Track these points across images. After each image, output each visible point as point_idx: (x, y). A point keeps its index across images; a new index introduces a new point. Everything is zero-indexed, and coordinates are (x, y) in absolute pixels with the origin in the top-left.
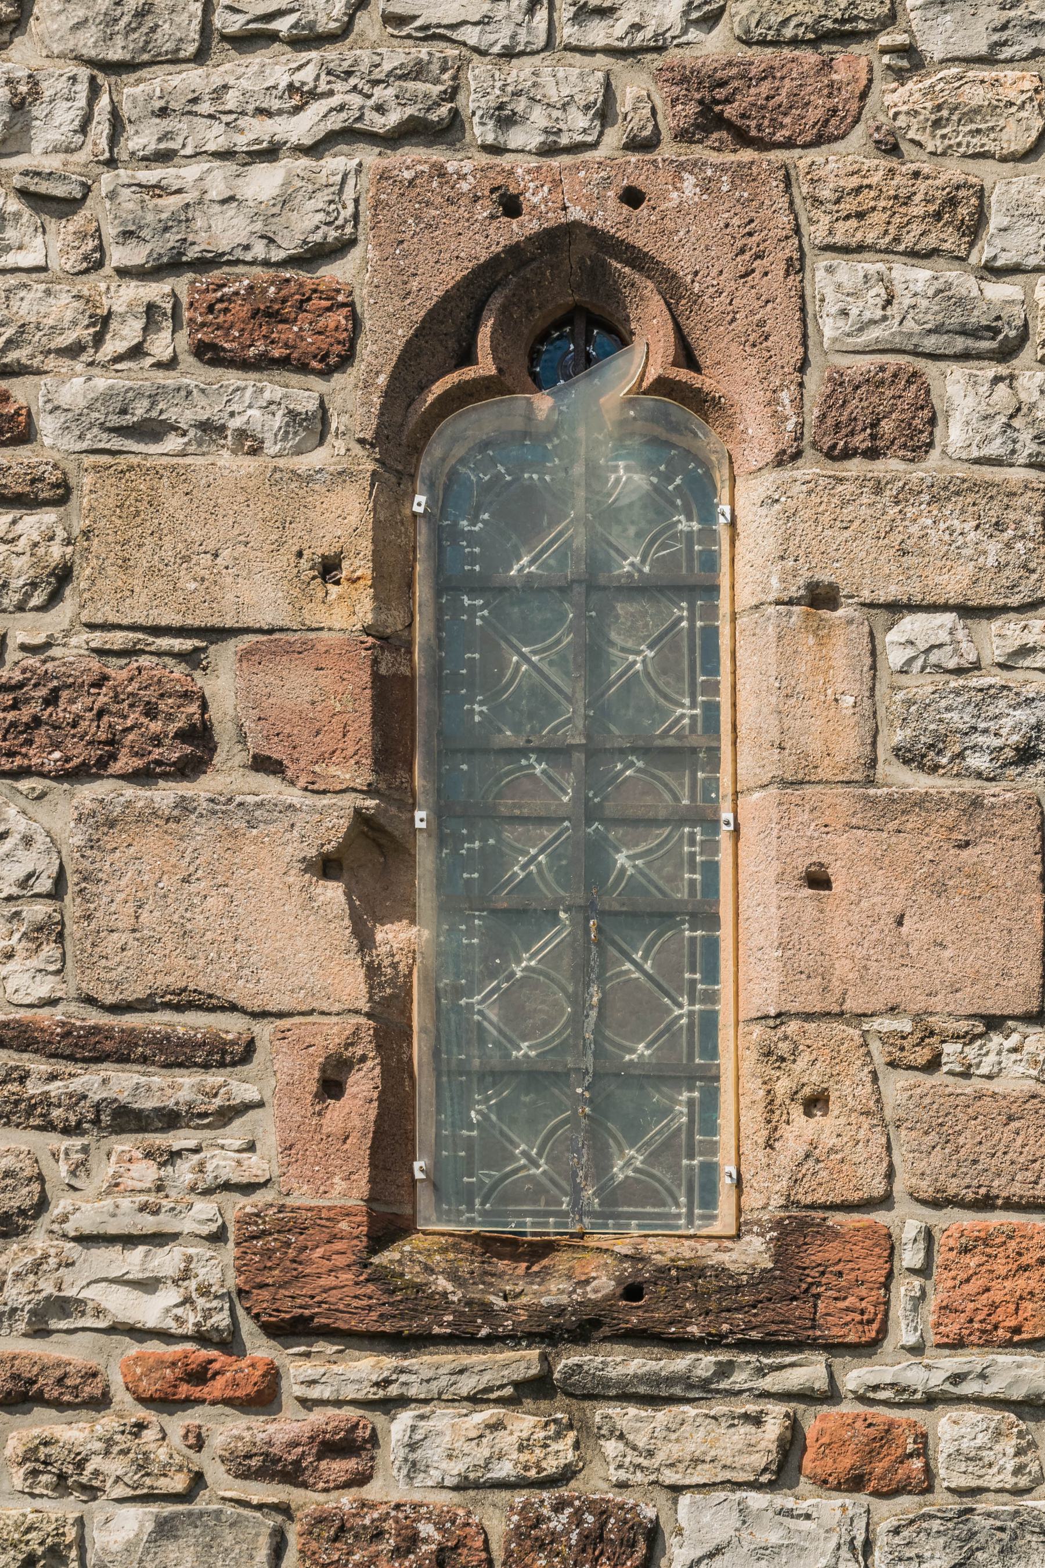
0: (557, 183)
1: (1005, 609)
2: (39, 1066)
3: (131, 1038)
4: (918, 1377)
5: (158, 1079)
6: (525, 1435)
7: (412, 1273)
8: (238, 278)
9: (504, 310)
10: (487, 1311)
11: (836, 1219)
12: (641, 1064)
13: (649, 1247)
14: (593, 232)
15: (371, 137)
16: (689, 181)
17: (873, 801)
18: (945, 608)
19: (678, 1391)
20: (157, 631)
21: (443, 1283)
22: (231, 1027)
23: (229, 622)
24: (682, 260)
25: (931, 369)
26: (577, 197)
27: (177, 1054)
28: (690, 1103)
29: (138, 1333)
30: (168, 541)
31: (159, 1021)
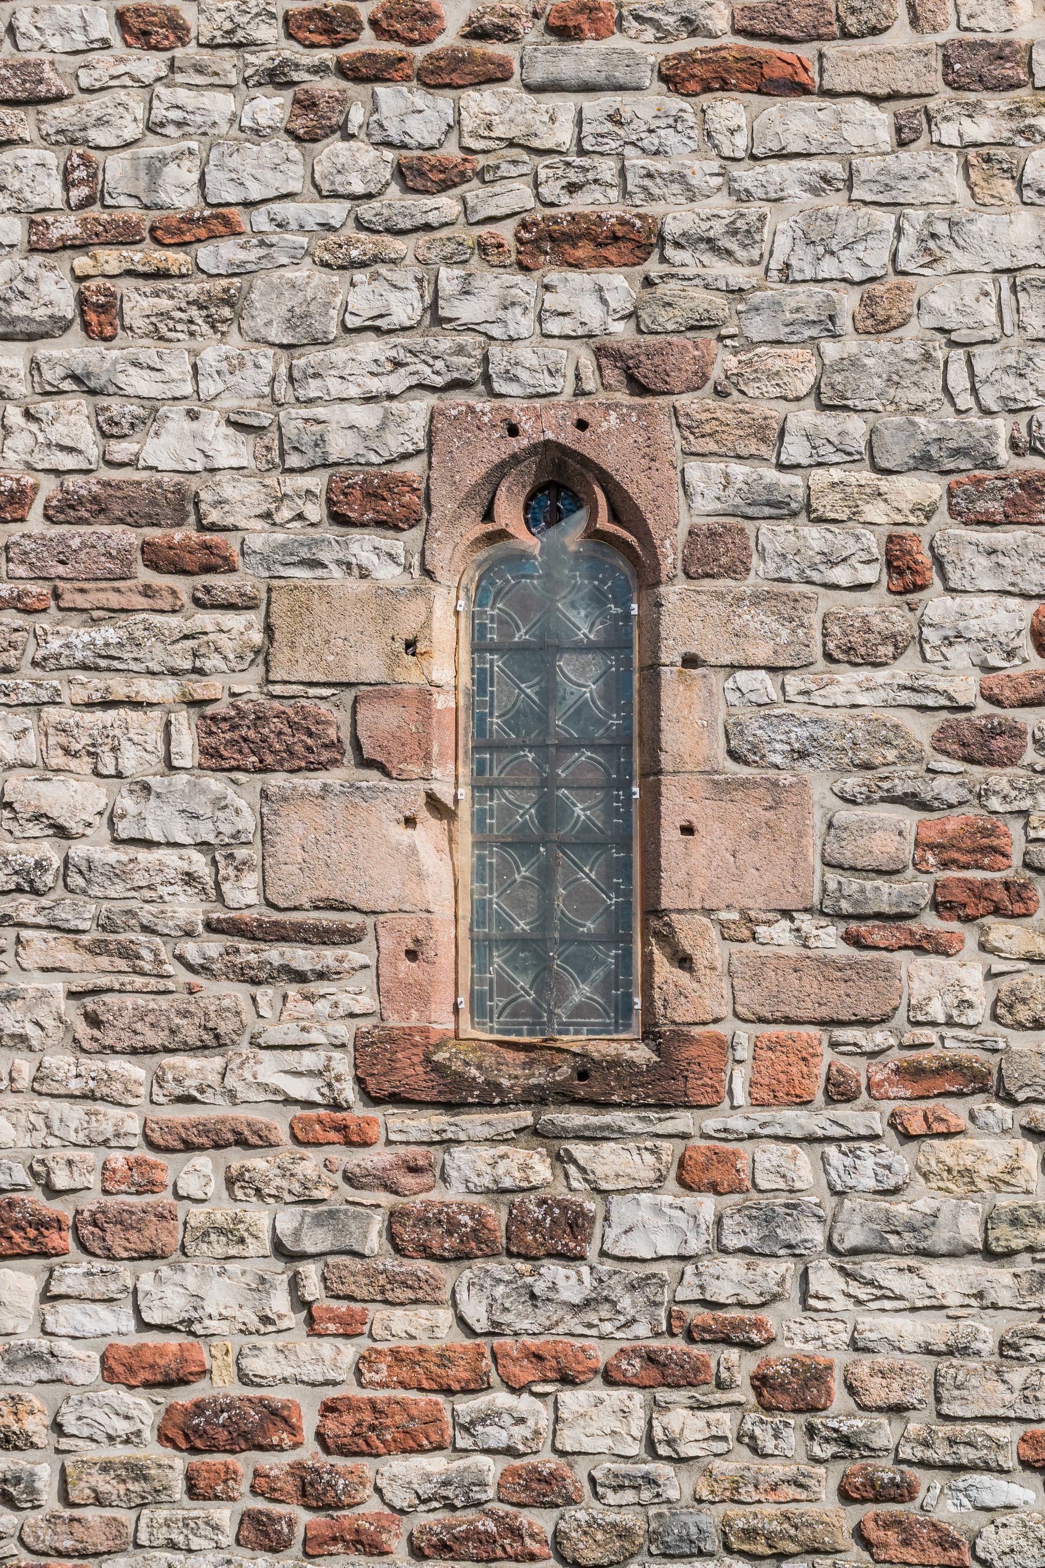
0: (539, 417)
1: (793, 668)
2: (244, 945)
3: (298, 927)
4: (738, 1123)
5: (311, 952)
6: (669, 1195)
7: (457, 1066)
8: (357, 473)
9: (509, 489)
10: (498, 1087)
11: (695, 1031)
12: (589, 934)
13: (591, 1047)
14: (558, 446)
15: (433, 389)
16: (613, 415)
17: (716, 783)
18: (758, 667)
19: (606, 1134)
20: (312, 684)
21: (474, 1072)
22: (352, 920)
23: (353, 680)
24: (609, 462)
25: (750, 527)
26: (551, 426)
27: (323, 936)
28: (616, 956)
29: (289, 1101)
30: (317, 631)
31: (311, 917)
